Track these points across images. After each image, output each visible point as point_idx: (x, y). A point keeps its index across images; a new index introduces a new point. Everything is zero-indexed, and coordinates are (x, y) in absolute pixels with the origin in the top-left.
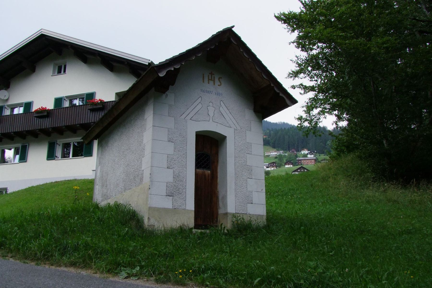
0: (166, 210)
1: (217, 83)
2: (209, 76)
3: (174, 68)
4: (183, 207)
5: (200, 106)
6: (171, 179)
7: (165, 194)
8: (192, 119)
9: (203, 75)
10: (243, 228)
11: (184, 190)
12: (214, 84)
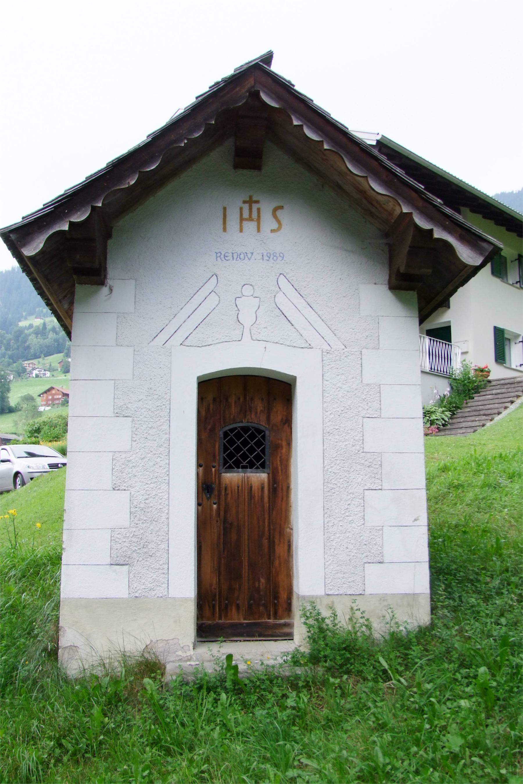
0: (110, 604)
1: (268, 222)
2: (241, 209)
3: (72, 224)
4: (161, 591)
5: (213, 299)
6: (123, 519)
7: (108, 561)
8: (187, 343)
9: (225, 209)
10: (343, 656)
11: (164, 546)
12: (259, 230)
